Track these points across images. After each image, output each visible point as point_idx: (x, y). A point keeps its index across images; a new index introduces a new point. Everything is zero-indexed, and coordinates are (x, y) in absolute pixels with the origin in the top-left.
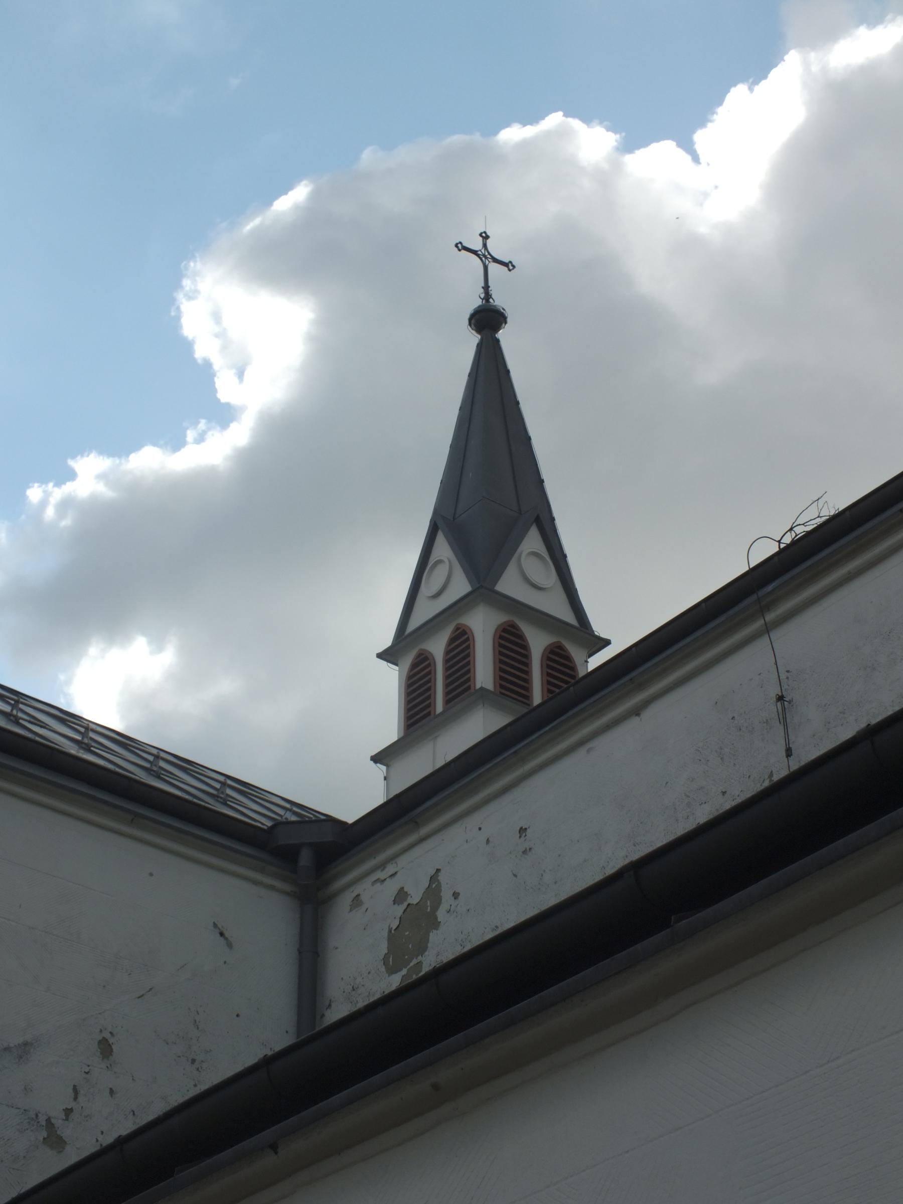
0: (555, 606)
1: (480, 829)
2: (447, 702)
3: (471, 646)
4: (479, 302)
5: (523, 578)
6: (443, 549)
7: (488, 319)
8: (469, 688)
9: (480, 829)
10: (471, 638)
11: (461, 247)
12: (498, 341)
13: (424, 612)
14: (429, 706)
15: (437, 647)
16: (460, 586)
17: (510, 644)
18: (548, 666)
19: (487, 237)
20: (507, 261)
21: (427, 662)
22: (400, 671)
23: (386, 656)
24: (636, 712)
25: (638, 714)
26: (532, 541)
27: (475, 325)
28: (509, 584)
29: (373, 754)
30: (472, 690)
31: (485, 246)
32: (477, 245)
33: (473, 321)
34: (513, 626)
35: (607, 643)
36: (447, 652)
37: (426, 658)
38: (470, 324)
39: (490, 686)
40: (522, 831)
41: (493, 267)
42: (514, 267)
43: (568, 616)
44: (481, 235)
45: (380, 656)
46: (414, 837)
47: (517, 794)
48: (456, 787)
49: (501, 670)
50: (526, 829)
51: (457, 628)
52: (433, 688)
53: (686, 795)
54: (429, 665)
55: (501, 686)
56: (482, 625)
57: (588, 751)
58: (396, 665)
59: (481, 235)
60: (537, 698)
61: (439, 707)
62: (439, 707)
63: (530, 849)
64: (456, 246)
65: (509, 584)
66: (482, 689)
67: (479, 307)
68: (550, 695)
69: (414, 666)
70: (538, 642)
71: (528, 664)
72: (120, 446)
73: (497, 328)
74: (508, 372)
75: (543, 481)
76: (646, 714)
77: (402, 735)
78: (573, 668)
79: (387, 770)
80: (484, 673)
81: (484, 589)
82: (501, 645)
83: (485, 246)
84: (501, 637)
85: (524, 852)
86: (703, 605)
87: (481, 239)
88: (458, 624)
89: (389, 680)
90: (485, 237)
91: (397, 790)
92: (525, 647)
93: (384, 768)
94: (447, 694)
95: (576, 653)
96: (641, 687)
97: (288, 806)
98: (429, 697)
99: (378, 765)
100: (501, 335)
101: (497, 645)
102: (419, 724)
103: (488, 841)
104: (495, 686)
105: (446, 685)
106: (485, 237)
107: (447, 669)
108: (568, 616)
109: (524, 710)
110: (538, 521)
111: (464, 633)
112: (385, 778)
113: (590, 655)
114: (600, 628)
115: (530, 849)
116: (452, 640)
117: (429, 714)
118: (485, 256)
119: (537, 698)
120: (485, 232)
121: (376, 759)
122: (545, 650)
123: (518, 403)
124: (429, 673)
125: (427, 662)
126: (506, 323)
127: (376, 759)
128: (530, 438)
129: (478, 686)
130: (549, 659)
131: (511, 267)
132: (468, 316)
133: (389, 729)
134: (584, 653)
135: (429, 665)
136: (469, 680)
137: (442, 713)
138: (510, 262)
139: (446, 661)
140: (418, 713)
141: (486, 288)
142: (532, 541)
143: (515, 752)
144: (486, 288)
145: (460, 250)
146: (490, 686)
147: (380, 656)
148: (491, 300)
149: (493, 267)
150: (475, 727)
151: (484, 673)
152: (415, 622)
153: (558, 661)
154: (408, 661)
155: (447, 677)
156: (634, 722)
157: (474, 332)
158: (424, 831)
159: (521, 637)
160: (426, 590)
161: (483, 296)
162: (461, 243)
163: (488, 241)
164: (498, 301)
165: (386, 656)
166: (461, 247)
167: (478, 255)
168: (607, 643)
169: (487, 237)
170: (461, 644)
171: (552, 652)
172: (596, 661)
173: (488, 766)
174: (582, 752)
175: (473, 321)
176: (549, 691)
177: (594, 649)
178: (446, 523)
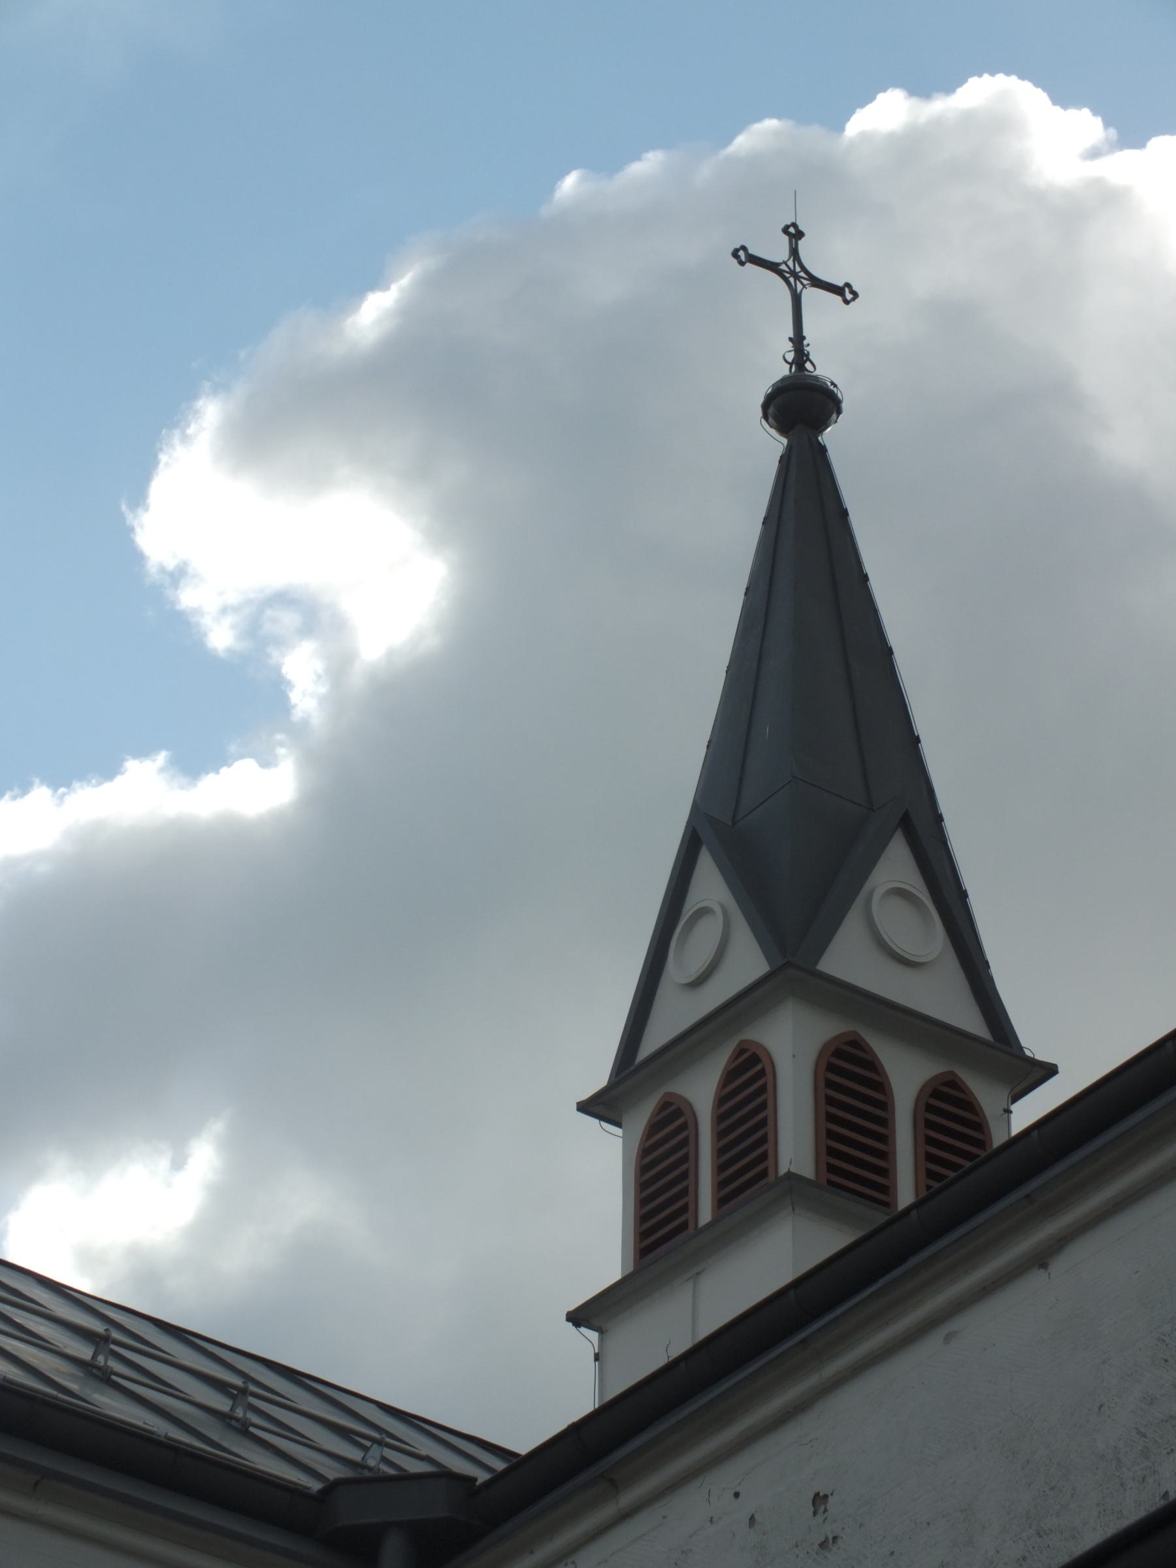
0: (945, 1000)
1: (737, 1495)
2: (721, 1202)
3: (770, 1087)
4: (784, 370)
5: (878, 945)
6: (710, 886)
7: (801, 406)
8: (764, 1174)
9: (737, 1495)
10: (768, 1070)
11: (744, 257)
12: (823, 450)
13: (674, 1016)
14: (684, 1209)
15: (701, 1089)
16: (747, 963)
17: (849, 1081)
18: (929, 1124)
19: (800, 235)
20: (841, 284)
21: (680, 1121)
22: (625, 1137)
23: (598, 1107)
24: (1040, 1259)
25: (1044, 1265)
26: (896, 867)
27: (775, 418)
28: (848, 958)
29: (571, 1308)
30: (771, 1178)
31: (794, 253)
32: (778, 251)
33: (771, 410)
34: (856, 1043)
35: (1049, 1071)
36: (721, 1100)
37: (678, 1113)
38: (765, 416)
39: (807, 1170)
40: (819, 1500)
41: (811, 296)
42: (855, 295)
43: (971, 1021)
44: (785, 230)
45: (585, 1107)
46: (812, 1380)
47: (808, 1425)
48: (750, 1370)
49: (831, 1135)
50: (826, 1497)
51: (740, 1051)
52: (770, 1122)
53: (1139, 1432)
54: (684, 1127)
55: (831, 1169)
56: (792, 1044)
57: (948, 1338)
58: (618, 1124)
59: (785, 230)
60: (905, 1194)
61: (705, 1214)
62: (705, 1214)
63: (835, 1538)
64: (735, 254)
65: (848, 958)
66: (790, 1175)
67: (784, 379)
68: (936, 1185)
69: (654, 1127)
70: (907, 1075)
71: (886, 1121)
72: (926, 83)
73: (822, 423)
74: (844, 513)
75: (917, 740)
76: (1060, 1265)
77: (631, 1269)
78: (980, 1126)
79: (602, 1341)
80: (795, 1144)
81: (794, 968)
82: (829, 1084)
83: (794, 253)
84: (831, 1068)
85: (823, 1545)
86: (1035, 1133)
87: (786, 238)
88: (742, 1042)
89: (603, 1162)
90: (794, 234)
91: (617, 1388)
92: (881, 1085)
93: (594, 1336)
94: (720, 1185)
95: (985, 1094)
96: (1049, 1210)
97: (375, 1435)
98: (684, 1192)
99: (583, 1329)
100: (830, 437)
101: (822, 1084)
102: (742, 1197)
103: (752, 1520)
104: (817, 1172)
105: (720, 1168)
106: (794, 234)
107: (719, 1135)
108: (971, 1021)
109: (881, 1218)
110: (906, 824)
111: (755, 1059)
112: (597, 1357)
113: (1015, 1098)
114: (1035, 1041)
115: (835, 1538)
116: (730, 1075)
117: (684, 1226)
118: (796, 276)
119: (905, 1194)
120: (794, 225)
121: (578, 1318)
122: (922, 1090)
123: (865, 578)
124: (685, 1143)
125: (680, 1121)
126: (839, 412)
127: (578, 1318)
128: (890, 651)
129: (783, 1170)
130: (929, 1108)
131: (849, 296)
132: (761, 399)
133: (605, 1260)
134: (1004, 1094)
135: (684, 1127)
136: (764, 1157)
137: (709, 1226)
138: (848, 285)
139: (719, 1118)
140: (662, 1228)
141: (798, 340)
142: (896, 867)
143: (802, 1342)
144: (798, 340)
145: (742, 264)
146: (807, 1170)
147: (585, 1107)
148: (808, 365)
149: (811, 296)
150: (773, 1258)
151: (795, 1144)
152: (652, 1042)
153: (950, 1114)
154: (641, 1117)
155: (719, 1152)
156: (1036, 1280)
157: (773, 432)
158: (628, 1498)
159: (873, 1065)
160: (675, 972)
161: (790, 357)
162: (744, 248)
163: (802, 243)
164: (825, 366)
165: (598, 1107)
166: (744, 257)
167: (780, 273)
168: (1049, 1071)
169: (800, 235)
170: (749, 1080)
171: (936, 1094)
172: (1027, 1112)
173: (750, 1370)
174: (933, 1343)
175: (771, 410)
176: (931, 1174)
177: (1018, 1089)
178: (721, 829)
